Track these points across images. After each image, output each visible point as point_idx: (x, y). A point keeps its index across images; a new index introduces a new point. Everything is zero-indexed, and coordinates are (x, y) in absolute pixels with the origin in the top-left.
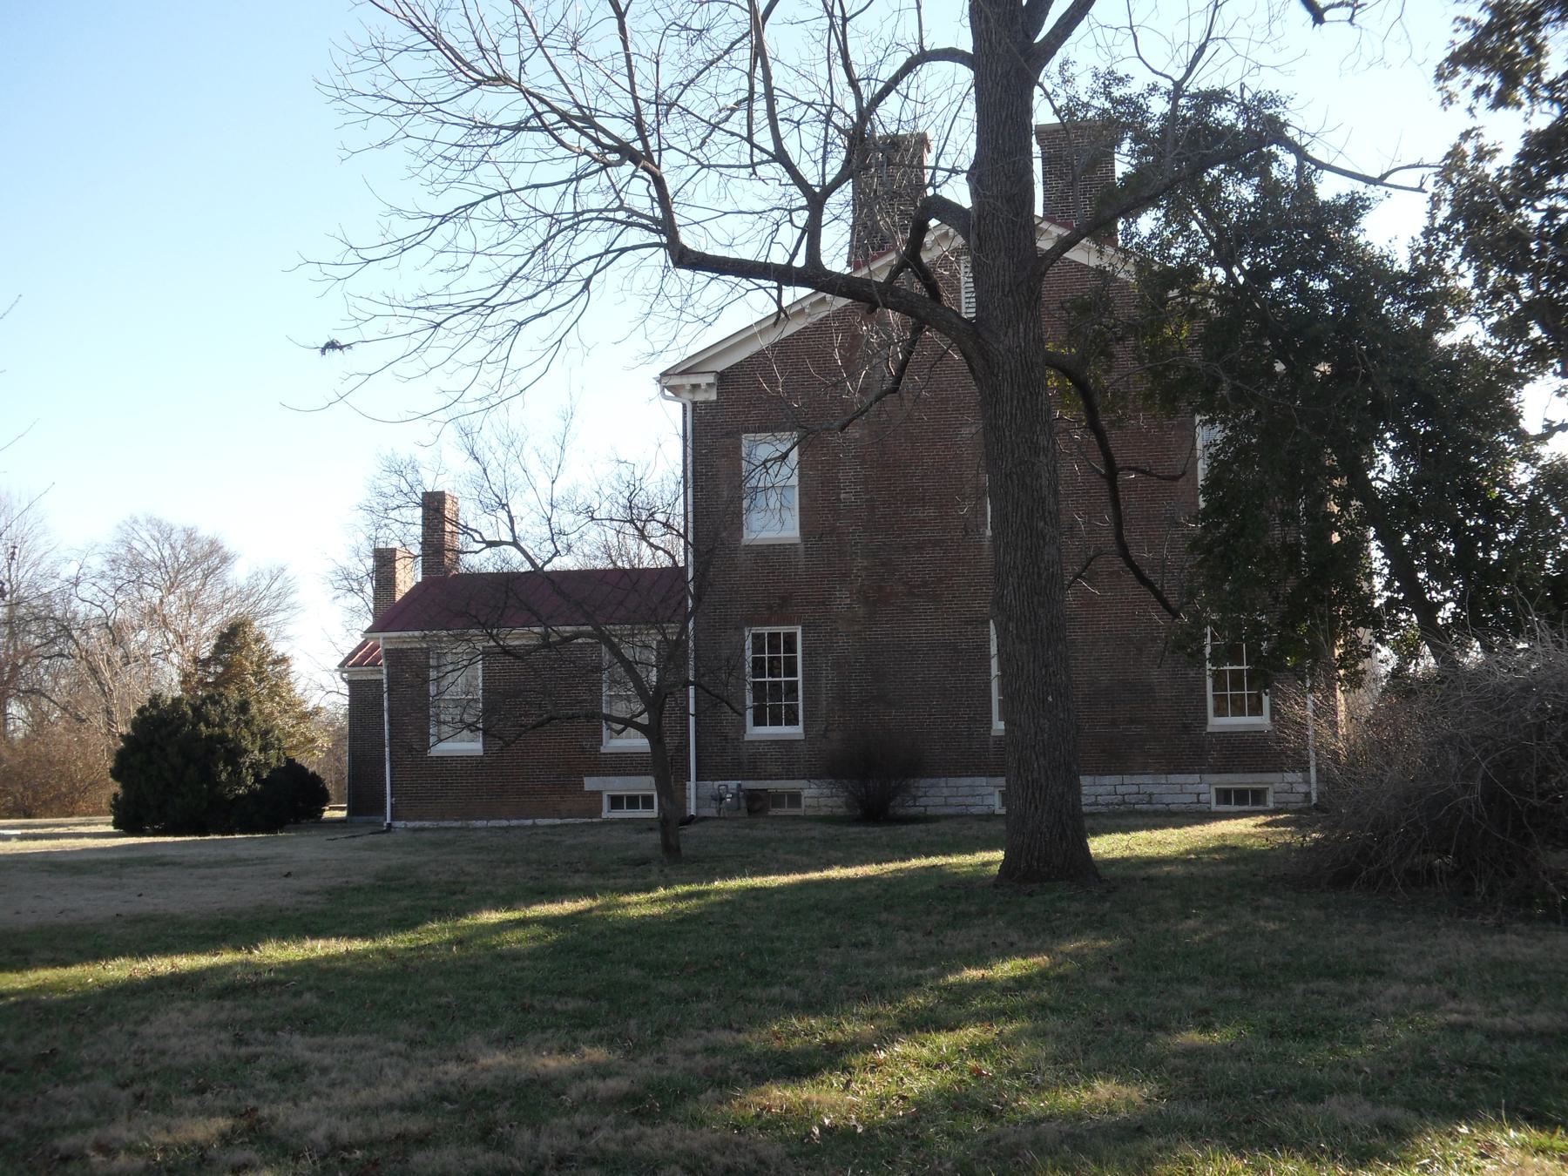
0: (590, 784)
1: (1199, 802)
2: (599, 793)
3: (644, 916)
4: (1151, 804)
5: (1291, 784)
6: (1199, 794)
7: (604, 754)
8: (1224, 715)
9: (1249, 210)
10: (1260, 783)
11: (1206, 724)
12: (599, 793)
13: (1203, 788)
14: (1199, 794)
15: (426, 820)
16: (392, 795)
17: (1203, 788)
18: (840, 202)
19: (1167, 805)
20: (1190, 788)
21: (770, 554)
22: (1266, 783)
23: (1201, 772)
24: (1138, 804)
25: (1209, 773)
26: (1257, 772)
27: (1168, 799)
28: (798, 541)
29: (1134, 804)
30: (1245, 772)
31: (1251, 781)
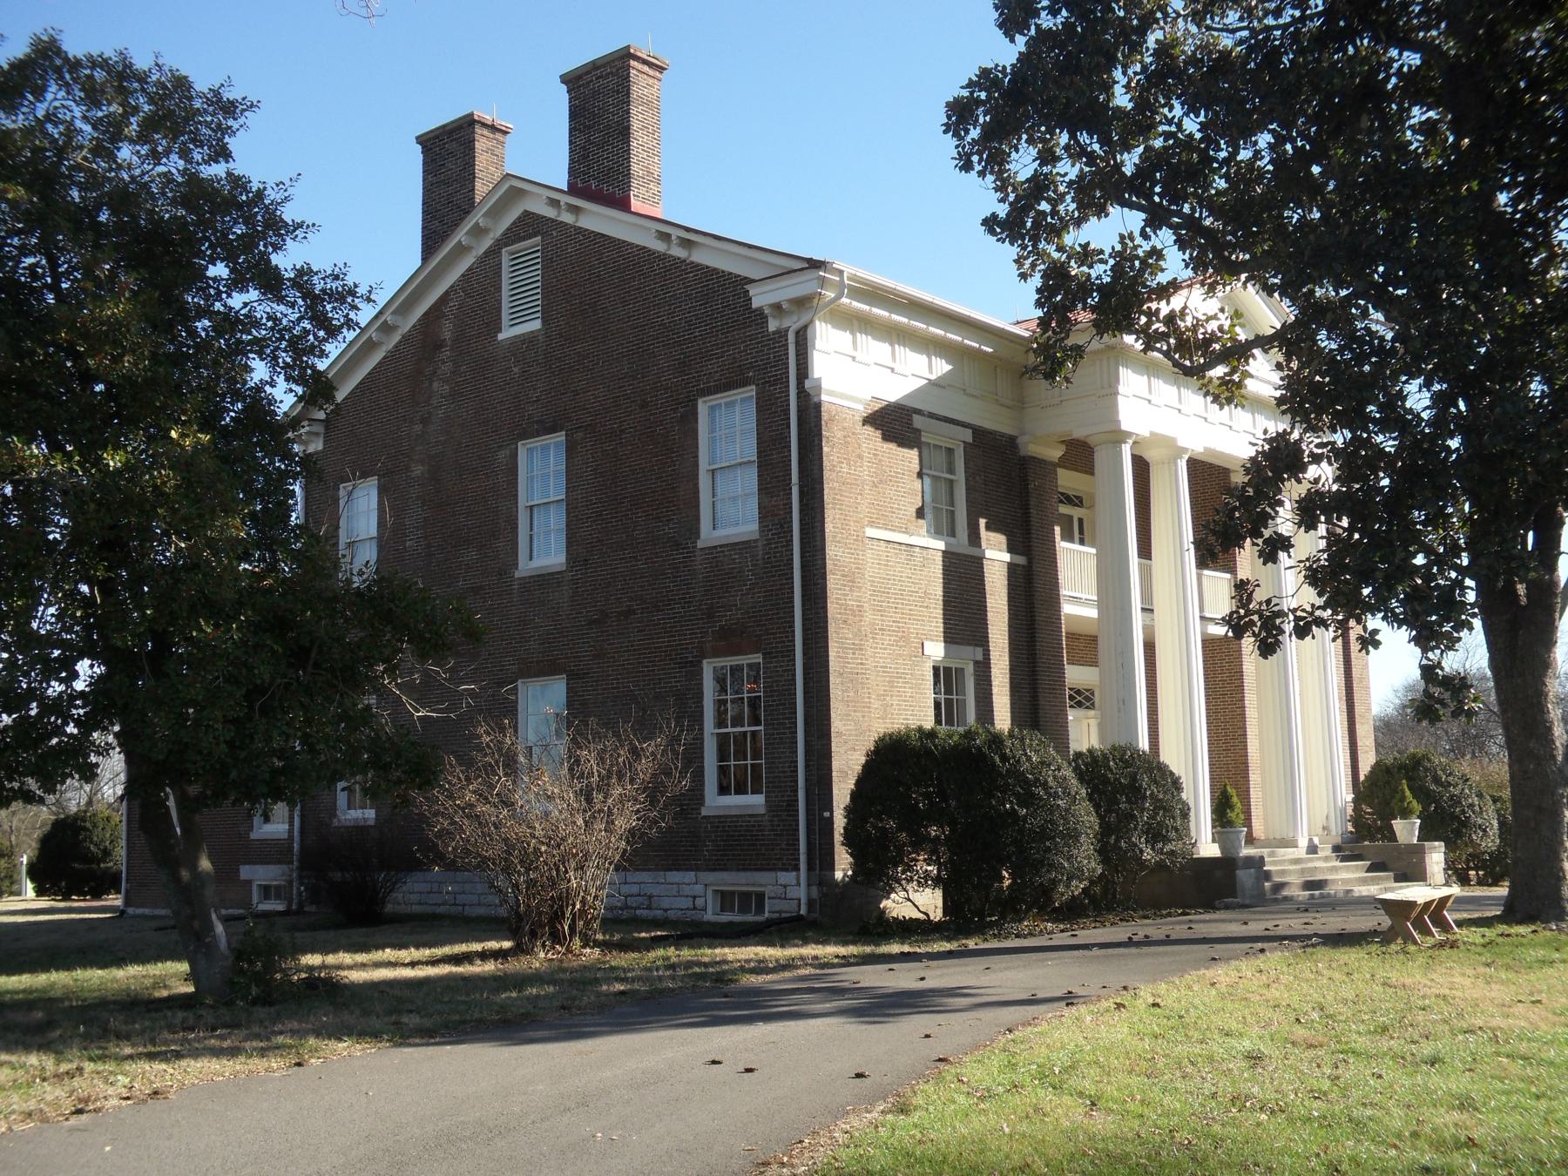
0: (246, 872)
1: (695, 908)
2: (249, 882)
3: (709, 947)
4: (650, 909)
5: (785, 887)
6: (695, 897)
7: (254, 840)
8: (744, 792)
9: (27, 169)
10: (753, 885)
11: (702, 804)
12: (249, 882)
13: (699, 889)
14: (695, 897)
15: (147, 907)
16: (128, 881)
17: (699, 889)
18: (1084, 138)
19: (666, 910)
20: (687, 890)
21: (545, 580)
22: (761, 885)
23: (697, 869)
24: (639, 908)
25: (704, 871)
26: (750, 870)
27: (665, 903)
28: (756, 536)
29: (636, 909)
30: (738, 870)
31: (744, 881)
